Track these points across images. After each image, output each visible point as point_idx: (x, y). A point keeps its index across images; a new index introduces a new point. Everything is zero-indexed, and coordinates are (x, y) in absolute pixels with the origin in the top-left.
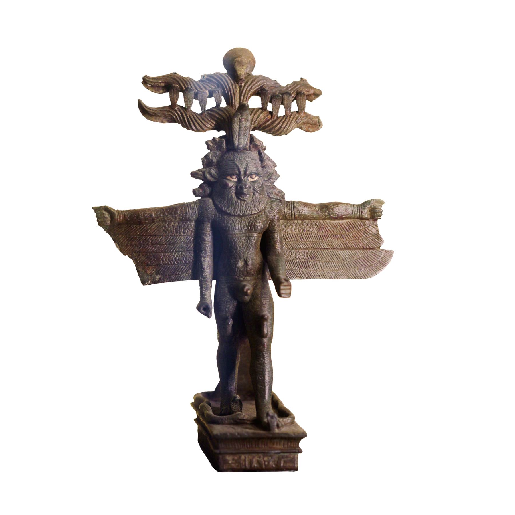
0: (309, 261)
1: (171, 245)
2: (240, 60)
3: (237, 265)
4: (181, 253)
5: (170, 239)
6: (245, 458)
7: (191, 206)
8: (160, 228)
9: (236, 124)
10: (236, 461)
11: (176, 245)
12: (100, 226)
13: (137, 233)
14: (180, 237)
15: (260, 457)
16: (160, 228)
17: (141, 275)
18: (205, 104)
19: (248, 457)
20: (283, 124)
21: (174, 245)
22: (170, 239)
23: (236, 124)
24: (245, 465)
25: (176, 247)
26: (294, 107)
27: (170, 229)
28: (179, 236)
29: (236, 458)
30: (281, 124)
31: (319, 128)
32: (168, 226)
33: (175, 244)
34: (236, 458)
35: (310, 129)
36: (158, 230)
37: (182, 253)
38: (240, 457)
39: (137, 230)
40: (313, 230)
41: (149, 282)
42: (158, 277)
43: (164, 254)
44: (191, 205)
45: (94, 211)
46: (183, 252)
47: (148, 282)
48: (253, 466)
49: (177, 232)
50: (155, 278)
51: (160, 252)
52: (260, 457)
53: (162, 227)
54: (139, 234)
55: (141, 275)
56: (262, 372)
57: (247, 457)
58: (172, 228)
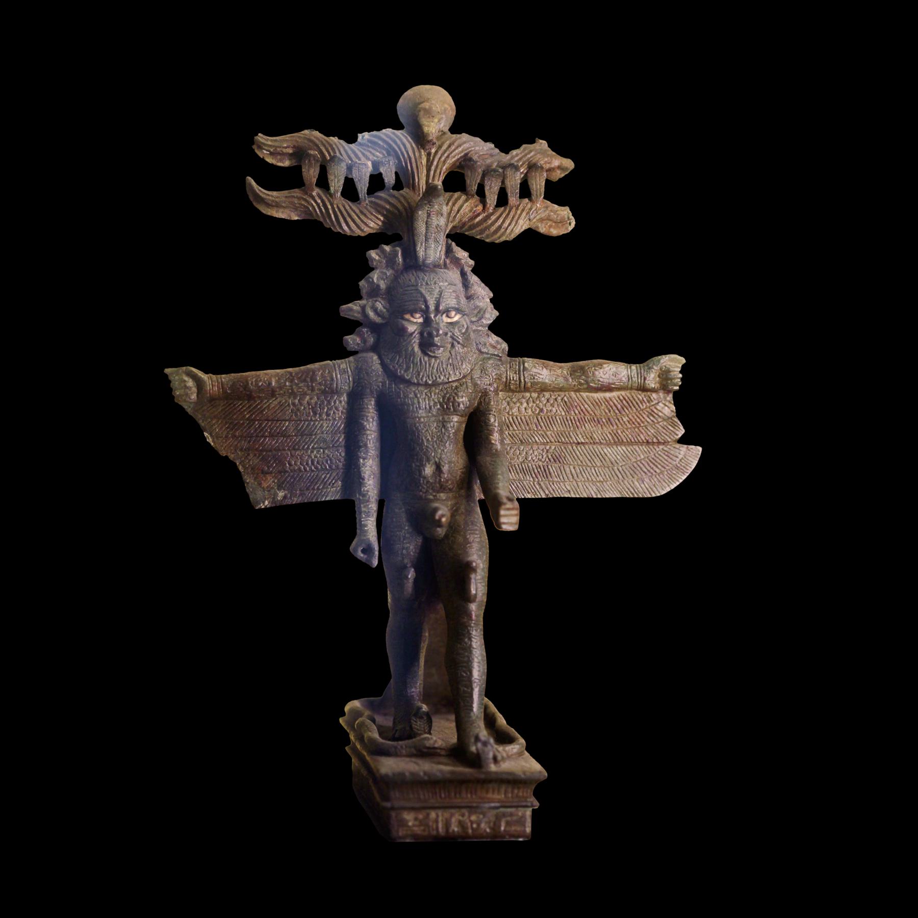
0: (551, 466)
1: (305, 437)
2: (427, 107)
3: (423, 473)
5: (302, 426)
6: (437, 816)
7: (341, 366)
8: (286, 407)
9: (420, 220)
10: (420, 821)
11: (314, 437)
13: (244, 416)
15: (463, 815)
16: (286, 407)
20: (504, 221)
21: (310, 437)
22: (302, 426)
23: (420, 220)
24: (437, 828)
25: (314, 439)
27: (303, 408)
28: (319, 421)
29: (421, 816)
32: (300, 403)
33: (312, 435)
34: (421, 816)
36: (282, 410)
37: (324, 452)
38: (428, 815)
39: (245, 410)
40: (558, 410)
43: (293, 452)
46: (326, 448)
48: (451, 831)
50: (276, 495)
52: (463, 815)
54: (247, 416)
57: (440, 814)
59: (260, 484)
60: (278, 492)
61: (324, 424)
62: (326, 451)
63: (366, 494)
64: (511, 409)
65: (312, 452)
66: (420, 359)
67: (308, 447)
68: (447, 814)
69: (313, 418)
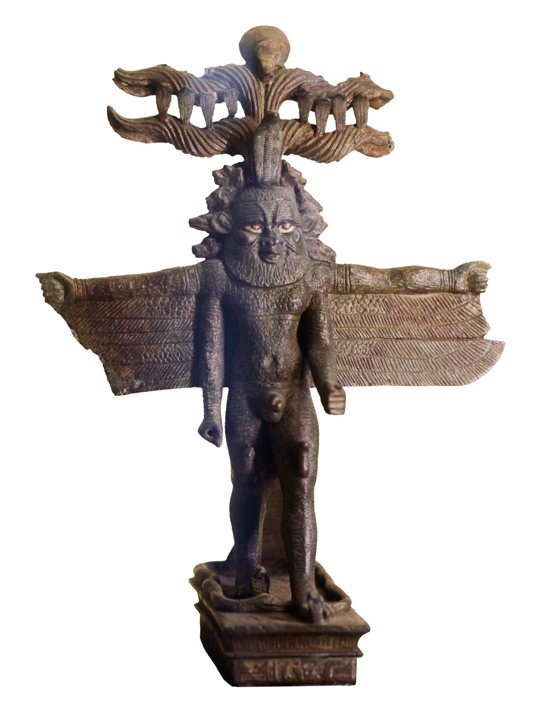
2: (265, 45)
4: (173, 345)
5: (156, 324)
6: (274, 664)
7: (190, 271)
10: (259, 669)
13: (106, 315)
15: (297, 664)
17: (112, 379)
18: (212, 114)
19: (279, 664)
20: (332, 145)
22: (156, 324)
27: (157, 308)
29: (260, 665)
31: (390, 151)
33: (165, 332)
34: (260, 665)
35: (374, 152)
37: (175, 346)
39: (106, 310)
40: (380, 310)
41: (125, 391)
43: (148, 346)
44: (189, 270)
46: (177, 343)
47: (123, 391)
49: (167, 313)
50: (133, 383)
51: (141, 344)
53: (144, 305)
54: (108, 315)
55: (112, 379)
58: (160, 306)
60: (135, 381)
69: (165, 316)
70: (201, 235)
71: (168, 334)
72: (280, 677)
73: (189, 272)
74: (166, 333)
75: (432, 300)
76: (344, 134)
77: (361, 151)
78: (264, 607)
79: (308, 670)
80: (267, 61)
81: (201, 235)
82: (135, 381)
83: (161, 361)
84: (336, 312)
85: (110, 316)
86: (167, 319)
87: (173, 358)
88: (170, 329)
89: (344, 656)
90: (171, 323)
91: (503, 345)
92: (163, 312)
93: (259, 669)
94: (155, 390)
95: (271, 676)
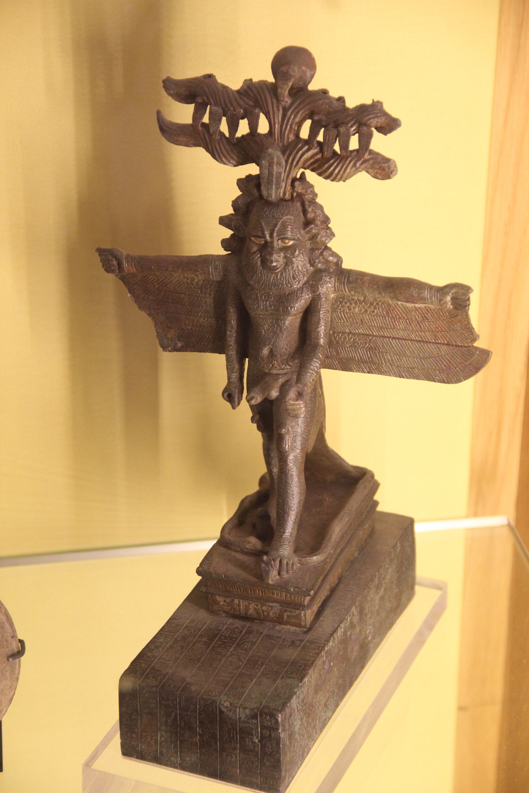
0: (372, 352)
1: (195, 307)
2: (285, 71)
3: (261, 355)
4: (206, 319)
5: (193, 300)
6: (239, 602)
7: (216, 262)
8: (182, 284)
9: (264, 168)
10: (228, 603)
11: (201, 308)
12: (236, 181)
13: (155, 286)
14: (205, 299)
15: (257, 606)
16: (182, 284)
17: (160, 338)
18: (236, 130)
19: (243, 602)
20: (334, 170)
21: (198, 308)
22: (193, 300)
23: (264, 168)
24: (239, 610)
25: (201, 310)
26: (354, 143)
27: (193, 287)
28: (205, 298)
29: (228, 601)
30: (332, 168)
31: (391, 176)
32: (191, 283)
33: (200, 307)
34: (228, 601)
35: (378, 175)
36: (180, 286)
37: (208, 320)
38: (233, 601)
39: (155, 282)
40: (379, 312)
41: (170, 349)
42: (179, 345)
43: (188, 316)
44: (216, 262)
45: (97, 254)
46: (209, 318)
47: (168, 348)
48: (249, 613)
49: (202, 292)
50: (176, 344)
51: (182, 314)
52: (257, 606)
53: (184, 283)
54: (157, 287)
55: (160, 338)
56: (283, 494)
57: (241, 601)
58: (196, 285)
59: (166, 335)
60: (177, 342)
61: (208, 301)
62: (210, 320)
63: (230, 357)
64: (343, 307)
65: (200, 319)
66: (261, 272)
67: (198, 314)
68: (246, 603)
69: (200, 295)
70: (227, 233)
71: (202, 309)
72: (245, 612)
73: (215, 262)
74: (201, 308)
75: (425, 310)
76: (346, 160)
77: (367, 172)
78: (246, 550)
79: (266, 611)
80: (282, 88)
81: (227, 233)
82: (177, 342)
83: (197, 330)
84: (340, 309)
85: (158, 287)
86: (201, 297)
87: (206, 329)
88: (204, 305)
89: (295, 609)
90: (205, 301)
91: (489, 355)
92: (198, 291)
93: (228, 603)
94: (193, 351)
95: (237, 611)
